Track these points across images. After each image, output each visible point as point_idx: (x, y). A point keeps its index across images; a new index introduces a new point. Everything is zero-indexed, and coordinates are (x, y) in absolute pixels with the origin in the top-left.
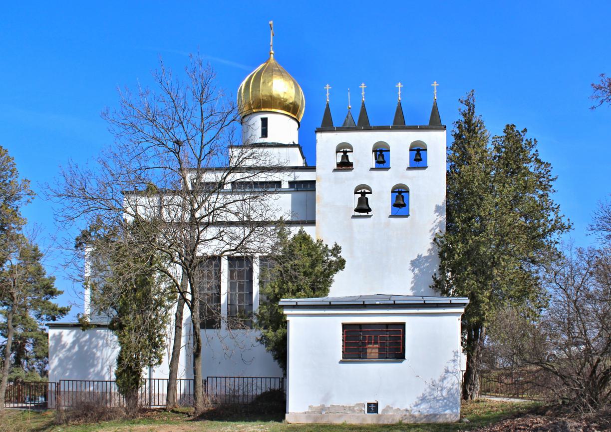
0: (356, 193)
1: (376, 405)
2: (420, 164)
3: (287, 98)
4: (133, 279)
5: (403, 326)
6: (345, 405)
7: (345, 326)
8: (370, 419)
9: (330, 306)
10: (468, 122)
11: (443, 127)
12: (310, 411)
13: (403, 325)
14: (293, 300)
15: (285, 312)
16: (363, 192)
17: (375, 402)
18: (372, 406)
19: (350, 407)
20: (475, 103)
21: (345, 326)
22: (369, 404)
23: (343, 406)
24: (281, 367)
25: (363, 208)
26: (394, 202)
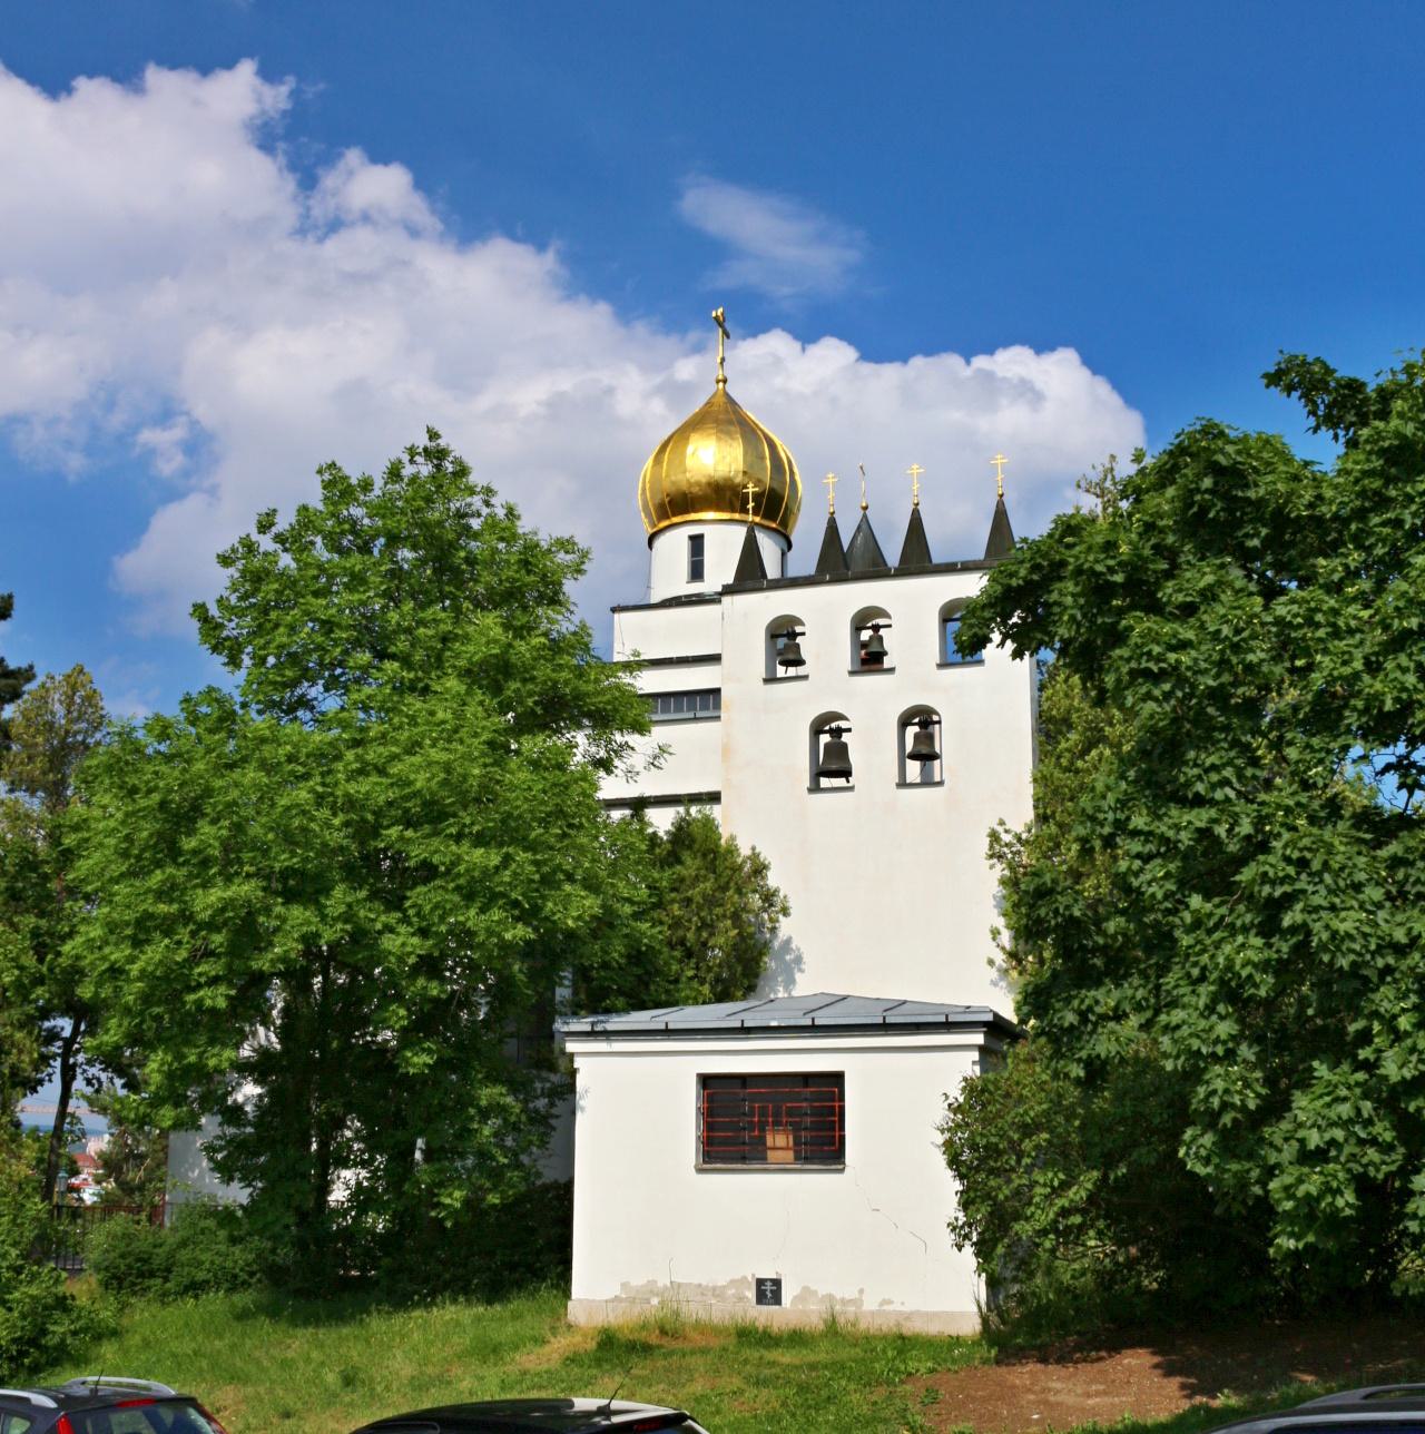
1: (777, 1283)
4: (1057, 774)
6: (704, 1283)
7: (706, 1081)
8: (764, 1316)
13: (837, 1078)
14: (583, 1025)
15: (571, 1047)
16: (827, 726)
19: (714, 1289)
21: (706, 1081)
22: (760, 1282)
23: (700, 1285)
25: (832, 764)
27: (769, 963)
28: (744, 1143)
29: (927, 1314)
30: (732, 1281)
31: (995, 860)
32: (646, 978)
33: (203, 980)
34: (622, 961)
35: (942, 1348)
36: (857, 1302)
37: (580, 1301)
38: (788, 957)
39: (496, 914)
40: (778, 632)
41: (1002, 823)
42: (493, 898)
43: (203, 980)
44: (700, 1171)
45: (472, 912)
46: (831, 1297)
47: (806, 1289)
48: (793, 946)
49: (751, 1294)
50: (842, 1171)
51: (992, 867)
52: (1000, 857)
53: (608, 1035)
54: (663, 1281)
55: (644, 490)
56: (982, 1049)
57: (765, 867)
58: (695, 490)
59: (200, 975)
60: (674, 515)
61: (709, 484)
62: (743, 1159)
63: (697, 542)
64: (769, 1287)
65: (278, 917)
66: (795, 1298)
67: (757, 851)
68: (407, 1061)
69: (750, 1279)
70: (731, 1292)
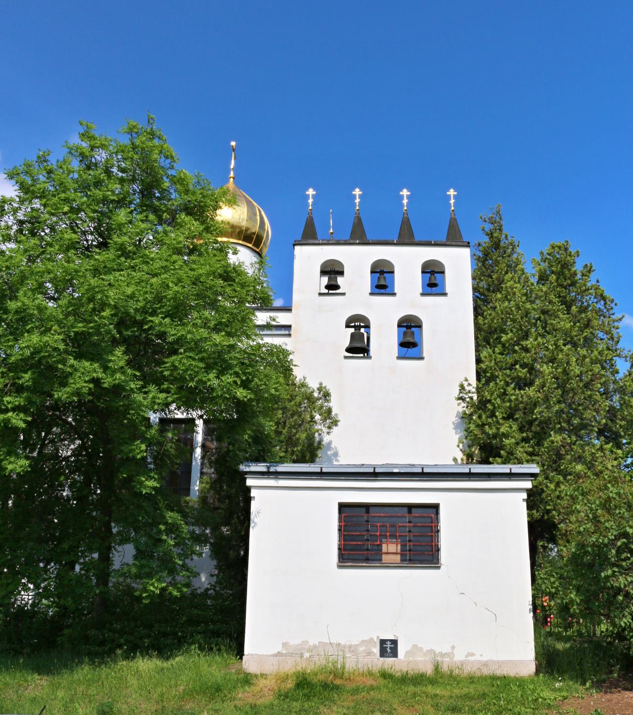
0: (348, 326)
1: (394, 642)
2: (412, 351)
3: (249, 227)
5: (434, 510)
6: (343, 643)
7: (342, 507)
9: (321, 475)
10: (496, 245)
11: (466, 244)
12: (284, 652)
13: (436, 507)
14: (261, 467)
17: (393, 638)
18: (389, 645)
19: (350, 647)
21: (342, 507)
22: (383, 642)
26: (401, 340)
27: (320, 453)
28: (367, 550)
29: (498, 662)
30: (363, 641)
31: (461, 401)
33: (9, 406)
34: (250, 440)
35: (520, 682)
36: (450, 655)
38: (329, 453)
41: (466, 380)
43: (9, 406)
46: (432, 651)
47: (415, 646)
48: (333, 446)
49: (376, 650)
51: (459, 404)
53: (277, 475)
56: (530, 492)
59: (9, 403)
62: (367, 560)
65: (72, 366)
66: (407, 652)
68: (141, 483)
69: (375, 640)
70: (362, 649)
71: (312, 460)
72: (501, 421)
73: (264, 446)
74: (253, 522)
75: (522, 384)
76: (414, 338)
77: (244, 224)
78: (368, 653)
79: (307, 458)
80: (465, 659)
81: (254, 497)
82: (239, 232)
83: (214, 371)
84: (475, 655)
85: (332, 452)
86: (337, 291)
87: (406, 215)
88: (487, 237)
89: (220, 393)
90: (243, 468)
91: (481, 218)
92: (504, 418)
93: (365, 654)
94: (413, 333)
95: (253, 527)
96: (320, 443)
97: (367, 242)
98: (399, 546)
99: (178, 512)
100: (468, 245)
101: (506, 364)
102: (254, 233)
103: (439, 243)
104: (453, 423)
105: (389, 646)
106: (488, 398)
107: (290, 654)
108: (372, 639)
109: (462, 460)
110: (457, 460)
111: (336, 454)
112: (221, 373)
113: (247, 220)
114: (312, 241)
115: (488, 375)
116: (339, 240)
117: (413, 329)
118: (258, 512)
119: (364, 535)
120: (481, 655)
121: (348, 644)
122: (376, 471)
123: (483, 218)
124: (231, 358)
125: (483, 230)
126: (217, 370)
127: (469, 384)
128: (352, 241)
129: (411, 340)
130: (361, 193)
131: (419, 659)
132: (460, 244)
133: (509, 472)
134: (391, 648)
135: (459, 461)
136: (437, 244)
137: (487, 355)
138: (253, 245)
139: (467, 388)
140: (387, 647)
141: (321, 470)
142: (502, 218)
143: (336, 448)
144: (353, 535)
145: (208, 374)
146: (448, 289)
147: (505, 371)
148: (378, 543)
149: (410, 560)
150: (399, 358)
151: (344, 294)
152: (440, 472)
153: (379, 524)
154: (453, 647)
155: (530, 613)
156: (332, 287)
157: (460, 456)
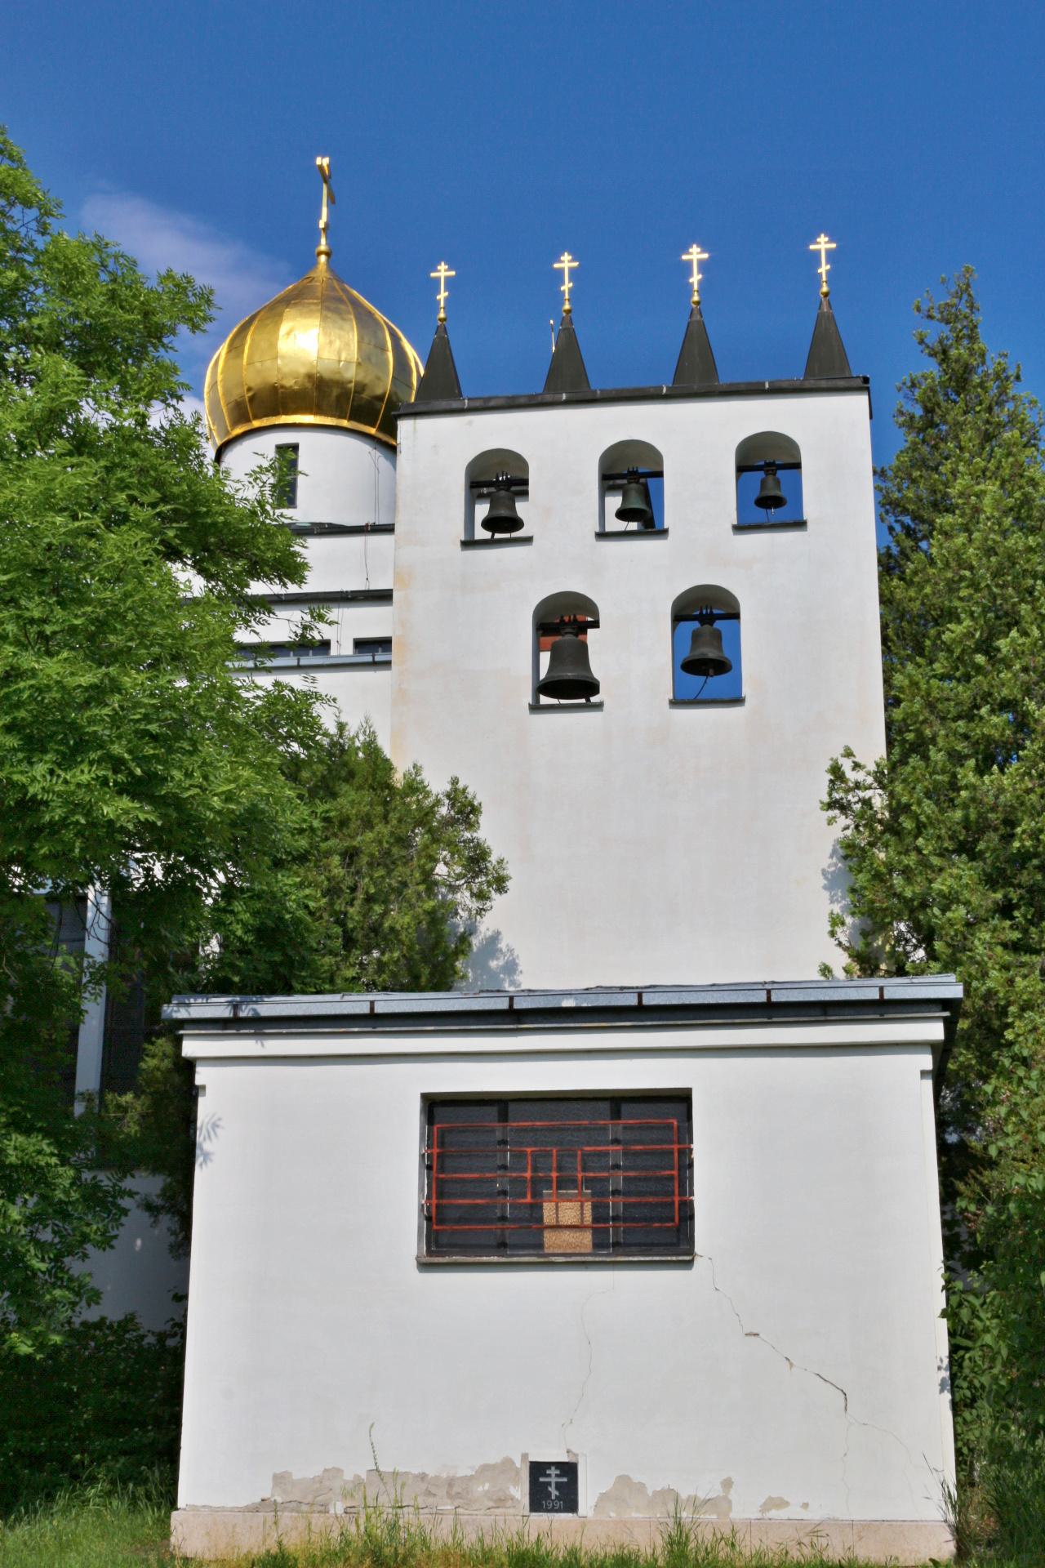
1: (569, 1470)
2: (716, 684)
3: (367, 381)
5: (682, 1107)
6: (431, 1473)
7: (433, 1105)
10: (960, 380)
11: (859, 383)
13: (682, 1099)
14: (218, 1007)
17: (564, 1459)
19: (451, 1482)
20: (978, 318)
21: (433, 1105)
22: (537, 1469)
23: (423, 1477)
24: (573, 1553)
28: (503, 1218)
29: (852, 1524)
30: (485, 1468)
31: (837, 812)
32: (988, 474)
34: (249, 938)
37: (194, 1508)
38: (493, 964)
39: (84, 774)
40: (482, 479)
41: (849, 753)
42: (77, 747)
44: (424, 1266)
45: (40, 769)
47: (624, 1480)
48: (502, 945)
49: (520, 1492)
50: (689, 1264)
51: (831, 821)
52: (844, 808)
53: (260, 1026)
54: (356, 1468)
55: (214, 385)
57: (475, 810)
58: (289, 383)
60: (256, 417)
61: (310, 376)
62: (502, 1246)
63: (288, 452)
64: (553, 1477)
66: (603, 1498)
67: (461, 786)
69: (518, 1465)
70: (483, 1488)
71: (442, 981)
72: (936, 861)
73: (291, 952)
74: (202, 1149)
75: (991, 756)
76: (720, 648)
77: (351, 374)
78: (500, 1500)
79: (423, 980)
80: (759, 1515)
81: (204, 1087)
82: (338, 398)
83: (48, 757)
84: (787, 1504)
85: (501, 962)
86: (515, 534)
87: (697, 317)
88: (933, 362)
89: (58, 814)
90: (175, 1011)
91: (919, 310)
92: (943, 853)
93: (491, 1504)
94: (718, 635)
95: (201, 1165)
96: (464, 939)
97: (589, 396)
98: (588, 1206)
99: (46, 1133)
100: (863, 385)
101: (956, 704)
102: (380, 398)
103: (785, 385)
104: (824, 872)
105: (553, 1480)
106: (904, 800)
107: (294, 1505)
108: (508, 1462)
109: (847, 970)
110: (830, 971)
111: (511, 968)
112: (68, 760)
113: (359, 364)
114: (443, 404)
115: (910, 736)
116: (513, 398)
117: (718, 624)
118: (215, 1126)
119: (493, 1181)
120: (805, 1506)
121: (444, 1475)
122: (516, 1006)
123: (924, 308)
124: (92, 721)
125: (922, 342)
126: (57, 752)
127: (857, 766)
128: (549, 398)
129: (711, 654)
130: (576, 264)
131: (634, 1515)
132: (841, 383)
133: (877, 997)
134: (559, 1486)
135: (839, 974)
136: (778, 390)
137: (907, 682)
138: (380, 429)
139: (852, 776)
140: (549, 1484)
141: (372, 1008)
142: (978, 304)
143: (511, 951)
144: (463, 1180)
145: (31, 764)
146: (809, 512)
147: (953, 725)
148: (529, 1199)
149: (616, 1244)
150: (676, 703)
151: (528, 540)
152: (693, 1002)
153: (529, 1150)
154: (727, 1484)
155: (942, 1391)
156: (504, 524)
157: (840, 960)
